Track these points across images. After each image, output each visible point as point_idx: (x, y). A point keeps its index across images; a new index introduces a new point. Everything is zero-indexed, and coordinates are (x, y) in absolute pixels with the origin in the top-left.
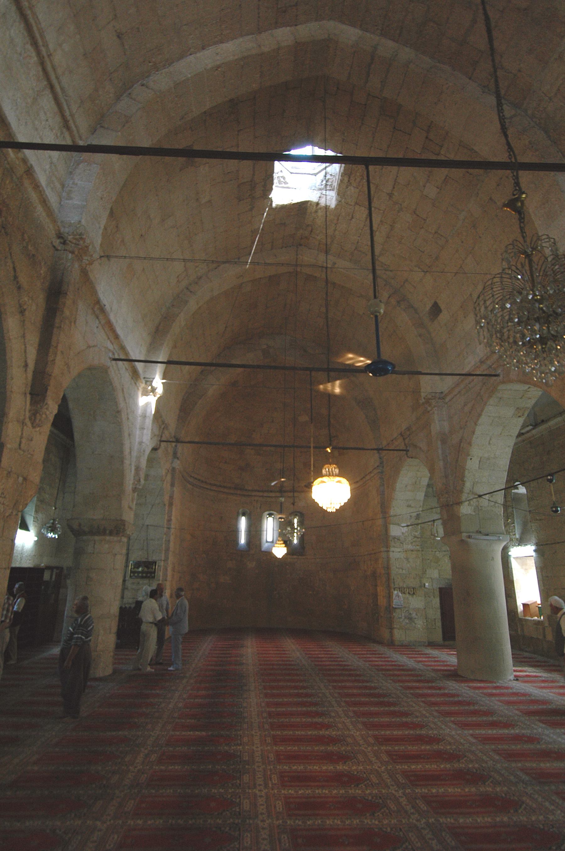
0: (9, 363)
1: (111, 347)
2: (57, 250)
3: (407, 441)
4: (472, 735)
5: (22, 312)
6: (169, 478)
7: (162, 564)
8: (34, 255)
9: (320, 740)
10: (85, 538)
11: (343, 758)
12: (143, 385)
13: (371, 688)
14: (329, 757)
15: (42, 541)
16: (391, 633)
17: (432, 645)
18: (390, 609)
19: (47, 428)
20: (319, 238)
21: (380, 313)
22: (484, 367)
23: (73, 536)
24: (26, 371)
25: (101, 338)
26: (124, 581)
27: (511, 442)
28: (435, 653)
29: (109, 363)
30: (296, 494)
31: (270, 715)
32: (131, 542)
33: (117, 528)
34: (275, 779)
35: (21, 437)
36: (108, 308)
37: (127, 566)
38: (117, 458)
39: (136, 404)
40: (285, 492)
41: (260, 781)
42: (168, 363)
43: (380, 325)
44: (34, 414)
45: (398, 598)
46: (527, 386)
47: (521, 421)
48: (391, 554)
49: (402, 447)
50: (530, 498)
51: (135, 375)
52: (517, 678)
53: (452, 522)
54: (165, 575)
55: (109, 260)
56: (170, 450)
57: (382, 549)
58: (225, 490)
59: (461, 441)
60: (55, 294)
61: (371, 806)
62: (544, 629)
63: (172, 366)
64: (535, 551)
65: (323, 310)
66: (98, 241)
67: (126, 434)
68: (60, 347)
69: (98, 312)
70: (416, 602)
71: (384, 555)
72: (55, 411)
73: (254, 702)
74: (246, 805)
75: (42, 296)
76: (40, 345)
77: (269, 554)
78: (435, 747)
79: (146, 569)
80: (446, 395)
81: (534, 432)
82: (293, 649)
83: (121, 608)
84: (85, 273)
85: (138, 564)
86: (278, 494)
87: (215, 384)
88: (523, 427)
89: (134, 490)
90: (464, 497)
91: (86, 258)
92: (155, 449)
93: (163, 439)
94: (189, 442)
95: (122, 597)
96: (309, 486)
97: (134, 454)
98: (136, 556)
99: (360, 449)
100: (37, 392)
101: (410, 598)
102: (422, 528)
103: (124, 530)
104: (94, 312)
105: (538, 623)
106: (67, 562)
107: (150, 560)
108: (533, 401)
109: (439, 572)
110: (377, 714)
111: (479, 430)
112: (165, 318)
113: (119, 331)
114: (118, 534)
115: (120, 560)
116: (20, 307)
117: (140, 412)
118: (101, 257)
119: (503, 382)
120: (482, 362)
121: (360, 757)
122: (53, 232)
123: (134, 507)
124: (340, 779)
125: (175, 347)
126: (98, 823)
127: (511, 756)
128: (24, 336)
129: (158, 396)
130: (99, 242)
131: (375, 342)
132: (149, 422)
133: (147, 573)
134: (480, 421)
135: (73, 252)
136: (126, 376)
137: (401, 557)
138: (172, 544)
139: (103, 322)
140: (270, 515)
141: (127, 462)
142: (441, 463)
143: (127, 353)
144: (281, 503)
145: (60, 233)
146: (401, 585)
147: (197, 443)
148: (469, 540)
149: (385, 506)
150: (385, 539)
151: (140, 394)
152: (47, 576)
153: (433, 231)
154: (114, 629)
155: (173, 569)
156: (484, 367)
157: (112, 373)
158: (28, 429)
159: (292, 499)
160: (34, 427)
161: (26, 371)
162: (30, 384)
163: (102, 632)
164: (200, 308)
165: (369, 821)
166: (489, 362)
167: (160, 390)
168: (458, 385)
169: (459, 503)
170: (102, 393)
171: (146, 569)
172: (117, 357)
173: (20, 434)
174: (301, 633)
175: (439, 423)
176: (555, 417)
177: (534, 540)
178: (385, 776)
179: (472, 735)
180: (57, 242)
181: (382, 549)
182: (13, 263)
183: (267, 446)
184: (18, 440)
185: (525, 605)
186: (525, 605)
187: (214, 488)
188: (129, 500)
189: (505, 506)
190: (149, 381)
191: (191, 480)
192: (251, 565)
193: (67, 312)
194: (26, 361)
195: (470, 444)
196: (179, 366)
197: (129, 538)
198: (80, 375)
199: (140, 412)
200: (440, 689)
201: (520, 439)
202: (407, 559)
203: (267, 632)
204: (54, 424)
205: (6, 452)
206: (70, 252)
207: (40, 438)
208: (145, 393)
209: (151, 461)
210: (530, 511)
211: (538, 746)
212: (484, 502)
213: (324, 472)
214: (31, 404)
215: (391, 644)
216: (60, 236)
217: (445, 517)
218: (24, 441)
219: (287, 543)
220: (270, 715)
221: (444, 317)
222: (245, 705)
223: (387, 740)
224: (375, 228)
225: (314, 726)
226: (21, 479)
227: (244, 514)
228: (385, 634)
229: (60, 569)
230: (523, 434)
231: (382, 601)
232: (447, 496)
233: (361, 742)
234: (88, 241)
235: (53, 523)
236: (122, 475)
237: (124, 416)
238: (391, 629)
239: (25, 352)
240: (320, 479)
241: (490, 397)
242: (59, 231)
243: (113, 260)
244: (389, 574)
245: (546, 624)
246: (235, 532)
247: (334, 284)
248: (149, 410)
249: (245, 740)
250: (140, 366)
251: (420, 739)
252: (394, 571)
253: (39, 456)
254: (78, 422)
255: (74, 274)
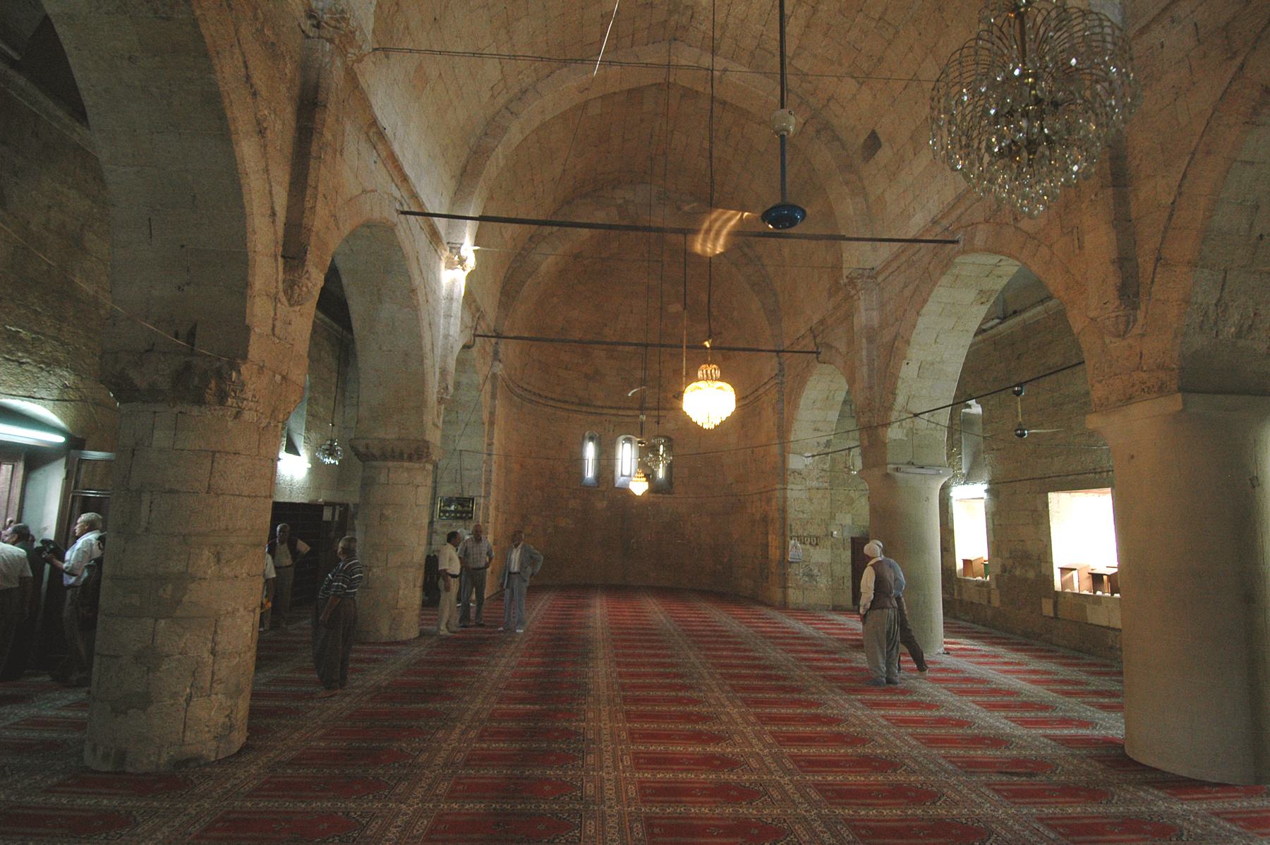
0: (248, 210)
1: (397, 194)
2: (308, 37)
3: (818, 340)
4: (883, 716)
5: (262, 132)
6: (488, 387)
7: (482, 500)
8: (273, 44)
9: (687, 717)
10: (375, 463)
11: (715, 738)
12: (447, 254)
13: (755, 658)
14: (697, 737)
15: (317, 466)
16: (785, 595)
17: (837, 609)
18: (784, 563)
19: (310, 306)
20: (703, 28)
21: (788, 131)
22: (938, 229)
23: (362, 459)
24: (273, 222)
25: (380, 177)
26: (431, 523)
27: (968, 340)
28: (841, 619)
29: (395, 218)
30: (662, 413)
31: (623, 687)
32: (439, 472)
33: (418, 452)
34: (627, 761)
35: (275, 319)
36: (389, 132)
37: (434, 504)
38: (413, 355)
39: (438, 281)
40: (647, 409)
41: (609, 763)
42: (480, 219)
43: (788, 168)
44: (290, 286)
45: (795, 549)
46: (998, 257)
47: (982, 311)
48: (789, 493)
49: (812, 347)
50: (987, 419)
51: (435, 236)
52: (947, 652)
53: (874, 448)
54: (487, 515)
55: (387, 57)
56: (489, 349)
57: (778, 486)
58: (566, 406)
59: (895, 339)
60: (308, 104)
61: (747, 794)
62: (989, 592)
63: (490, 224)
64: (987, 491)
65: (706, 144)
66: (369, 24)
67: (425, 323)
68: (321, 188)
69: (375, 139)
70: (820, 556)
71: (778, 494)
72: (321, 283)
73: (601, 672)
74: (590, 789)
75: (289, 109)
76: (291, 184)
77: (625, 491)
78: (835, 729)
79: (460, 508)
80: (878, 273)
81: (1001, 327)
82: (655, 611)
83: (428, 557)
84: (352, 77)
85: (449, 502)
86: (637, 412)
87: (548, 259)
88: (986, 320)
89: (441, 401)
90: (894, 415)
91: (352, 51)
92: (466, 347)
93: (480, 332)
94: (515, 338)
95: (430, 543)
96: (679, 396)
97: (438, 351)
98: (446, 490)
99: (753, 350)
100: (293, 253)
101: (812, 549)
102: (833, 460)
103: (428, 454)
104: (369, 139)
105: (982, 585)
106: (353, 498)
107: (466, 496)
108: (1005, 281)
109: (854, 515)
110: (760, 689)
111: (922, 322)
112: (475, 153)
113: (408, 170)
114: (419, 458)
115: (424, 495)
116: (259, 124)
117: (444, 292)
118: (375, 50)
119: (964, 252)
120: (935, 222)
121: (737, 738)
122: (301, 7)
123: (440, 424)
124: (709, 762)
125: (491, 198)
126: (403, 806)
127: (932, 741)
128: (267, 170)
129: (469, 270)
130: (371, 27)
131: (779, 171)
132: (457, 307)
133: (462, 512)
134: (924, 311)
135: (331, 41)
136: (423, 239)
137: (804, 496)
138: (494, 476)
139: (384, 154)
140: (628, 440)
141: (428, 362)
142: (865, 369)
143: (421, 205)
144: (642, 423)
145: (311, 10)
146: (800, 532)
147: (527, 339)
148: (897, 474)
149: (783, 431)
150: (782, 473)
151: (443, 265)
152: (327, 514)
153: (877, 16)
154: (420, 582)
155: (497, 509)
156: (938, 229)
157: (401, 233)
158: (283, 308)
159: (656, 417)
160: (291, 305)
161: (273, 222)
162: (281, 243)
163: (403, 585)
164: (525, 139)
165: (747, 811)
166: (945, 223)
167: (471, 263)
168: (897, 257)
169: (887, 425)
170: (397, 277)
171: (463, 507)
172: (406, 209)
173: (272, 313)
174: (664, 592)
175: (866, 314)
176: (1033, 305)
177: (986, 477)
178: (768, 760)
179: (883, 716)
180: (307, 25)
181: (778, 486)
182: (243, 54)
183: (624, 344)
184: (271, 321)
185: (966, 562)
186: (966, 562)
187: (551, 403)
188: (433, 414)
189: (951, 430)
190: (455, 248)
191: (519, 392)
192: (601, 505)
193: (328, 136)
194: (272, 208)
195: (908, 342)
196: (496, 224)
197: (436, 467)
198: (353, 233)
199: (444, 292)
200: (845, 661)
201: (980, 337)
202: (810, 500)
203: (619, 590)
204: (320, 305)
205: (253, 339)
206: (327, 40)
207: (301, 322)
208: (450, 266)
209: (461, 362)
210: (984, 438)
211: (969, 731)
212: (921, 423)
213: (700, 373)
214: (285, 272)
215: (784, 607)
216: (311, 14)
217: (866, 443)
218: (278, 324)
219: (650, 476)
220: (623, 687)
221: (885, 154)
222: (591, 675)
223: (772, 719)
224: (787, 12)
225: (679, 701)
226: (278, 378)
227: (591, 439)
228: (777, 595)
229: (345, 506)
230: (985, 331)
231: (774, 553)
232: (869, 417)
233: (739, 720)
234: (353, 23)
235: (331, 445)
236: (422, 381)
237: (421, 299)
238: (785, 588)
239: (271, 193)
240: (694, 385)
241: (943, 273)
242: (309, 5)
243: (395, 57)
244: (784, 519)
245: (993, 586)
246: (579, 461)
247: (724, 103)
248: (456, 290)
249: (591, 715)
250: (440, 224)
251: (816, 719)
252: (792, 514)
253: (302, 344)
254: (357, 306)
255: (336, 76)
